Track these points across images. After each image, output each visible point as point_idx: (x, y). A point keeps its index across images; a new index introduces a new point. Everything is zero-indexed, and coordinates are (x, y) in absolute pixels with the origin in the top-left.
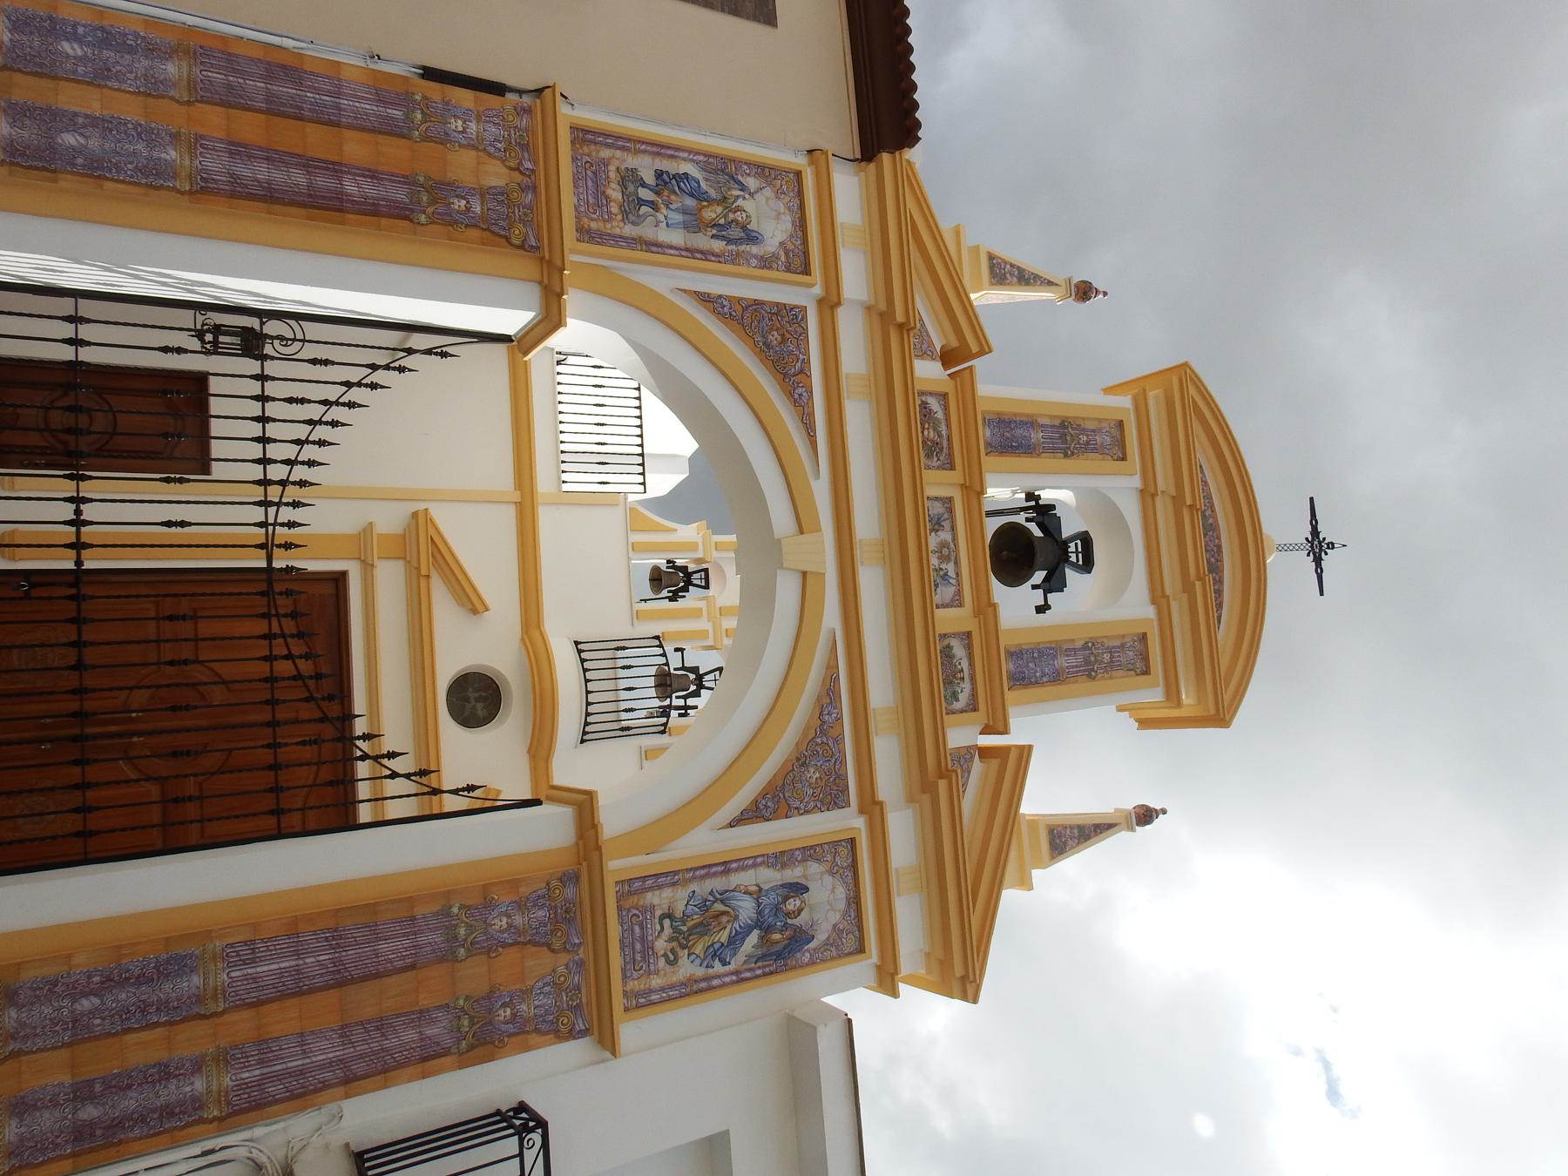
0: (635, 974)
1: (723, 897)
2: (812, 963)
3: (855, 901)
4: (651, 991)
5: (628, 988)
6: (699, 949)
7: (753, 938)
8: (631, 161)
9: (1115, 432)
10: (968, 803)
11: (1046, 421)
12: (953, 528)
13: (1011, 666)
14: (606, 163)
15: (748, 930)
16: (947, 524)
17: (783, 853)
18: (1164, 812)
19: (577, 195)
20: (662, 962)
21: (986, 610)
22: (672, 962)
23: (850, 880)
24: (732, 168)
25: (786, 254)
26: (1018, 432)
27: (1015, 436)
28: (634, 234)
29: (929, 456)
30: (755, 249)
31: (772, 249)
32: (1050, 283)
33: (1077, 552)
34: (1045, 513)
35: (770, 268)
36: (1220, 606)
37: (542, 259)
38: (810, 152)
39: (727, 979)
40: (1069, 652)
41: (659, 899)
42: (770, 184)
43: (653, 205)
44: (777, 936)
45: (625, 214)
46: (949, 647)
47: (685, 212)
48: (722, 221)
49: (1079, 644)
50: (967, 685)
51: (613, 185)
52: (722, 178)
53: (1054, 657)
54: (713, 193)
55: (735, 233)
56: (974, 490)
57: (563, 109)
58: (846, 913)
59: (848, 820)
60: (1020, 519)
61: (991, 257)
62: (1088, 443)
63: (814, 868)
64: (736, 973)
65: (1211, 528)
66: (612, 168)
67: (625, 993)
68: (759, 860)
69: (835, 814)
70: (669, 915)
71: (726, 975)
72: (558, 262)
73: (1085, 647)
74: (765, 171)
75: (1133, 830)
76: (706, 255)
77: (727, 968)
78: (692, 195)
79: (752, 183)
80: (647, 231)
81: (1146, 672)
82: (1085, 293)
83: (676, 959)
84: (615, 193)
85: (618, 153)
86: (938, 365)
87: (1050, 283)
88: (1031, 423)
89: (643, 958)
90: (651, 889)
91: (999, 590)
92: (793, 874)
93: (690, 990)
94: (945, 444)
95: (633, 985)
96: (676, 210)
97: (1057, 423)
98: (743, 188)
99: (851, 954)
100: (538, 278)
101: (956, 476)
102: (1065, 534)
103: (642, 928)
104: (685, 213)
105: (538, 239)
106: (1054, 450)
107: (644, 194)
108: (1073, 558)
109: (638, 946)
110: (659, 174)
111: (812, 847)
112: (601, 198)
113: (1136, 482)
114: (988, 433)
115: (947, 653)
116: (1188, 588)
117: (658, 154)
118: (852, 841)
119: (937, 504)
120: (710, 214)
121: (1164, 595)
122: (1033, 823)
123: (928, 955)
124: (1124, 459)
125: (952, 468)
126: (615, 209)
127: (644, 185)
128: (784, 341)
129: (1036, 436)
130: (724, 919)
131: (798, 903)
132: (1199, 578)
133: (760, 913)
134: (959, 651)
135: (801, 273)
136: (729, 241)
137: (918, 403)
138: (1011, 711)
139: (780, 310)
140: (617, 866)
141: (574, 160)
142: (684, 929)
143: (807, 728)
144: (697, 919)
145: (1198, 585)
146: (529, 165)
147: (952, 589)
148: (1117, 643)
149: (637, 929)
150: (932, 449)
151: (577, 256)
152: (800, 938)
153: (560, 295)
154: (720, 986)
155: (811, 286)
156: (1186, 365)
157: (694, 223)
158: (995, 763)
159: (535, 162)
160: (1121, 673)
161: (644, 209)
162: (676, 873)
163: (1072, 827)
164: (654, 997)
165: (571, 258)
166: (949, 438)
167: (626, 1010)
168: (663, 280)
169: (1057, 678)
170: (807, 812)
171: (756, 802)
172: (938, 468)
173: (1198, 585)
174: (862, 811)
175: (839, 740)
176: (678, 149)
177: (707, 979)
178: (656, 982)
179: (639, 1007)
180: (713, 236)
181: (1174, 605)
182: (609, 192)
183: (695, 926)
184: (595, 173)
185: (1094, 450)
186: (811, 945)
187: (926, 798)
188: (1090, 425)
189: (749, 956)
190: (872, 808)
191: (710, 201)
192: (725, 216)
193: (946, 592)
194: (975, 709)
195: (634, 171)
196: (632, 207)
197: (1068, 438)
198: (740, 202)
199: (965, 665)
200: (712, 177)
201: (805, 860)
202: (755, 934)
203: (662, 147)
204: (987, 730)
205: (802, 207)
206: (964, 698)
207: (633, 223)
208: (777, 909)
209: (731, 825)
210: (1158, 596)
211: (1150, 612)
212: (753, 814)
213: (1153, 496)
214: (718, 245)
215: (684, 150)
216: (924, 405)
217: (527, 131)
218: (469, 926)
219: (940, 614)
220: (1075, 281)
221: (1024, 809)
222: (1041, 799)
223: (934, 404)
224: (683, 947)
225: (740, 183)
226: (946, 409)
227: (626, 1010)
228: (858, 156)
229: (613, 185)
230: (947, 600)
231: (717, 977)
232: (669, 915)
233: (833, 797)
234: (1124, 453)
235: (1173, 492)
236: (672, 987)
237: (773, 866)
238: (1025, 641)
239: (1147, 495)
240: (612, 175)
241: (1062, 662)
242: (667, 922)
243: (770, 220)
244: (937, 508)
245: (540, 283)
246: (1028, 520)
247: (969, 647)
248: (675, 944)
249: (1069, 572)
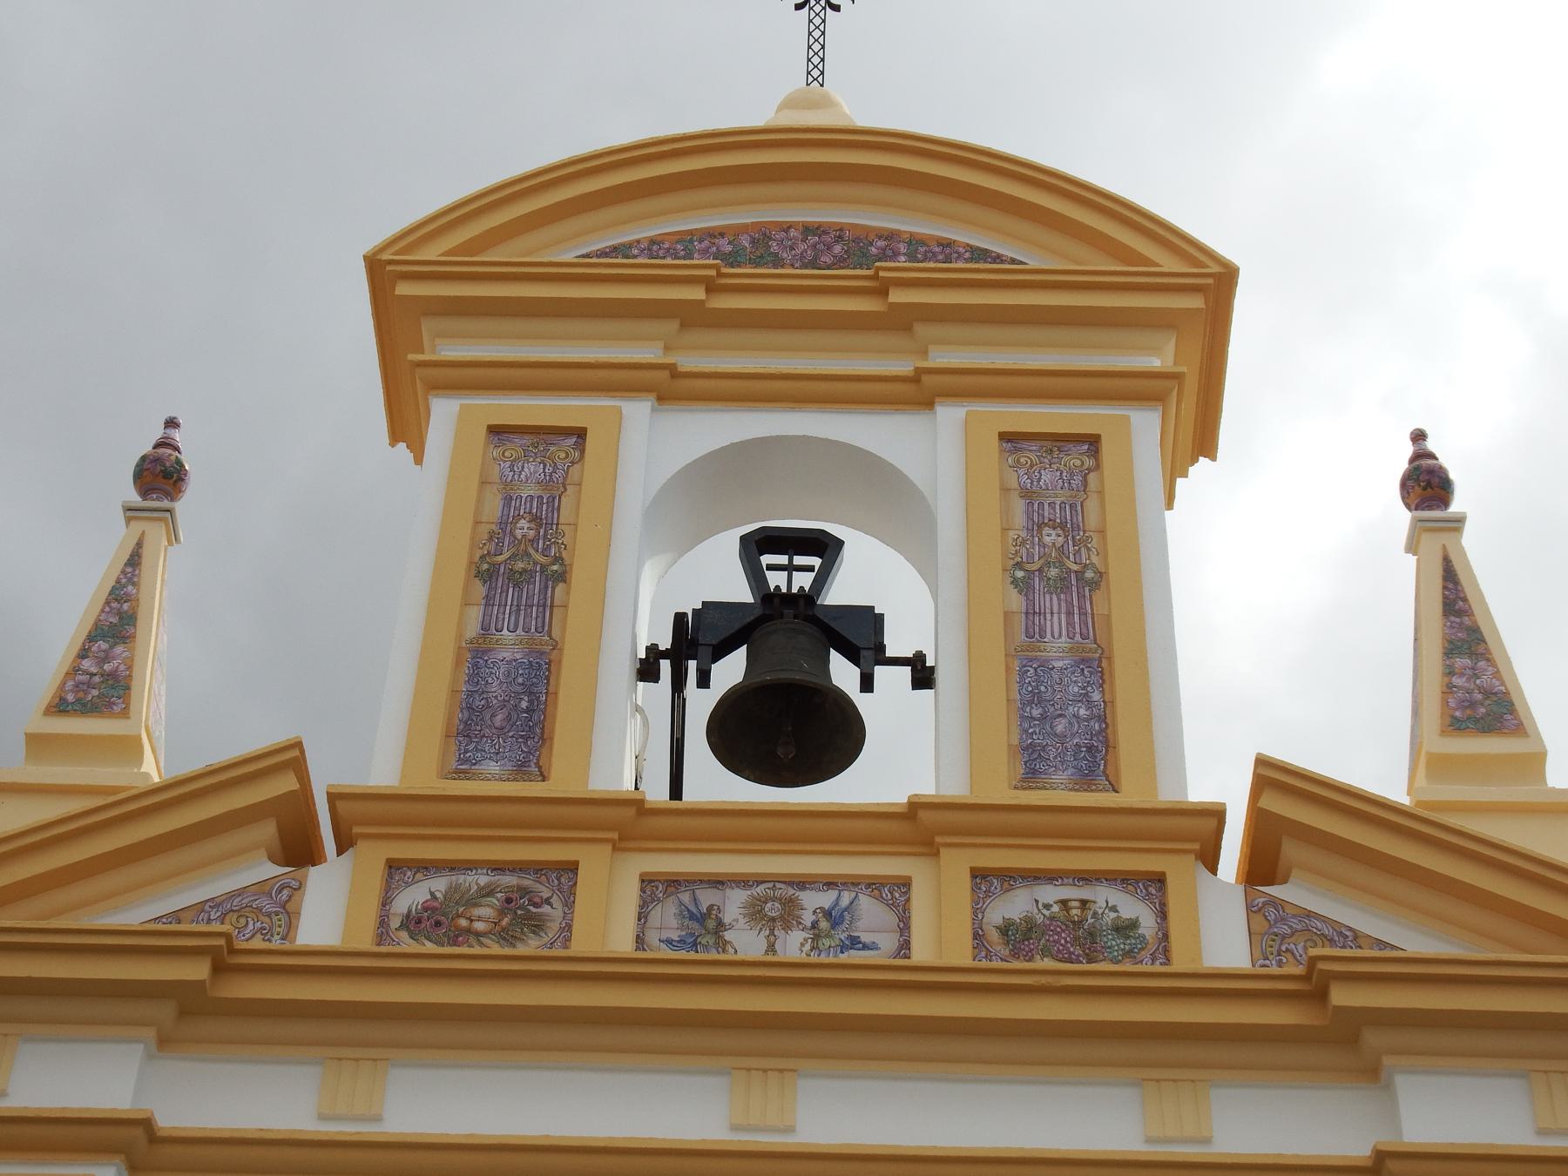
9: (515, 447)
10: (1415, 941)
11: (475, 614)
12: (718, 882)
13: (1061, 777)
16: (707, 898)
18: (1419, 436)
21: (918, 826)
26: (495, 688)
27: (505, 700)
29: (537, 925)
32: (134, 560)
33: (790, 568)
34: (696, 639)
36: (947, 249)
40: (1035, 632)
46: (1006, 929)
49: (1016, 601)
50: (1102, 895)
53: (1044, 665)
56: (626, 822)
60: (701, 704)
61: (59, 707)
62: (536, 519)
65: (762, 245)
73: (1024, 587)
75: (1458, 522)
81: (1092, 443)
82: (167, 475)
86: (314, 872)
87: (134, 560)
88: (477, 655)
91: (872, 781)
94: (510, 880)
97: (480, 590)
101: (593, 861)
102: (741, 593)
106: (546, 605)
108: (803, 581)
113: (637, 412)
114: (492, 767)
115: (1020, 936)
116: (902, 322)
119: (656, 915)
121: (916, 377)
122: (1427, 763)
124: (580, 434)
125: (572, 868)
129: (509, 645)
132: (882, 291)
134: (1015, 905)
137: (407, 944)
138: (1166, 795)
145: (897, 296)
147: (866, 903)
148: (1019, 506)
150: (521, 915)
156: (382, 272)
158: (1291, 850)
160: (1092, 506)
163: (1450, 672)
166: (498, 867)
169: (1094, 664)
172: (569, 904)
173: (897, 296)
181: (942, 358)
185: (554, 503)
187: (1373, 1039)
188: (493, 507)
193: (872, 917)
194: (1159, 880)
197: (520, 568)
199: (1050, 894)
204: (1210, 860)
206: (1130, 907)
210: (917, 394)
211: (950, 416)
213: (674, 372)
216: (413, 923)
219: (921, 953)
220: (134, 498)
221: (1398, 794)
222: (1371, 747)
223: (412, 897)
226: (426, 867)
230: (891, 919)
234: (565, 432)
235: (672, 326)
238: (1003, 734)
239: (672, 389)
241: (1057, 646)
244: (667, 919)
246: (704, 681)
247: (1011, 878)
249: (835, 595)
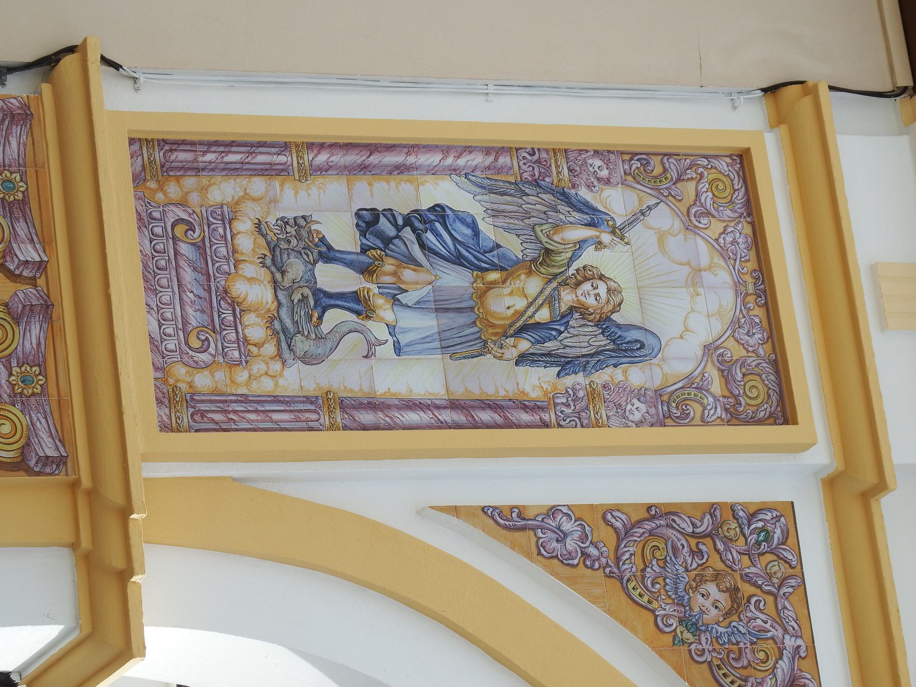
8: (293, 200)
14: (227, 216)
19: (157, 310)
24: (561, 174)
25: (726, 376)
28: (311, 388)
30: (636, 376)
31: (685, 368)
35: (683, 419)
37: (74, 485)
38: (771, 90)
42: (665, 196)
43: (357, 303)
45: (284, 338)
47: (441, 306)
48: (543, 315)
51: (250, 270)
52: (535, 202)
54: (513, 246)
55: (582, 339)
57: (114, 99)
66: (244, 226)
72: (113, 493)
74: (650, 166)
76: (504, 413)
78: (458, 260)
79: (616, 201)
80: (344, 373)
84: (254, 289)
85: (258, 185)
96: (419, 306)
98: (594, 217)
100: (69, 537)
104: (441, 309)
105: (62, 437)
107: (333, 278)
110: (368, 221)
112: (222, 306)
117: (364, 168)
120: (507, 302)
126: (255, 329)
127: (328, 255)
128: (737, 604)
135: (773, 419)
136: (566, 364)
139: (719, 523)
141: (144, 221)
146: (29, 253)
151: (162, 464)
153: (124, 575)
155: (806, 447)
157: (470, 333)
159: (45, 241)
161: (334, 317)
165: (145, 471)
168: (395, 489)
176: (412, 148)
178: (242, 381)
180: (523, 359)
182: (239, 288)
184: (200, 247)
191: (508, 268)
192: (551, 301)
195: (301, 223)
196: (303, 315)
198: (589, 257)
200: (507, 203)
203: (373, 148)
205: (758, 241)
207: (307, 359)
214: (536, 381)
215: (429, 148)
217: (21, 166)
218: (745, 644)
225: (585, 208)
228: (904, 79)
229: (250, 270)
240: (246, 242)
243: (672, 290)
245: (74, 546)
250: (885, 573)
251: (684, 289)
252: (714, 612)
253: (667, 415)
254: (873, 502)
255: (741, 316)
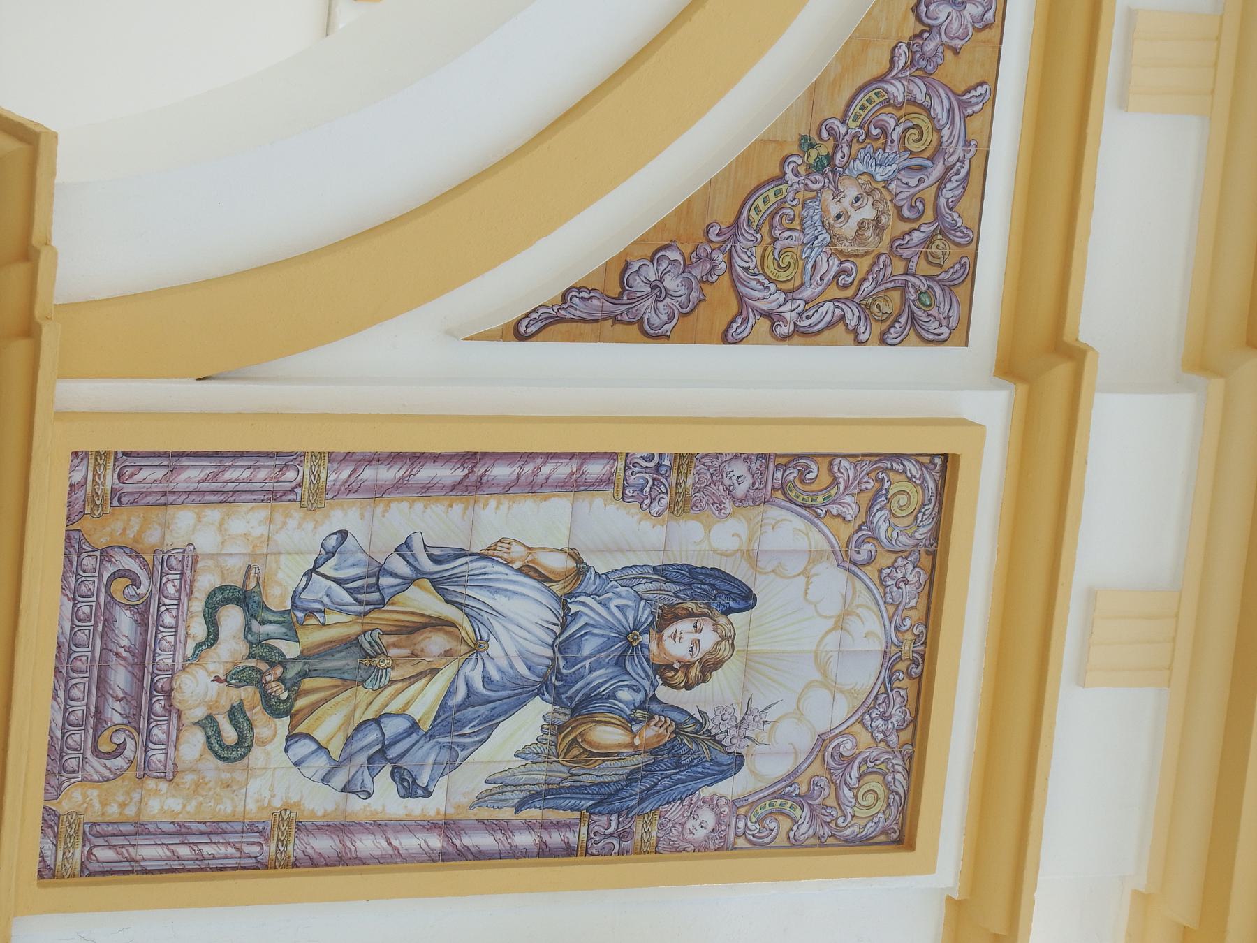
0: (96, 766)
1: (445, 570)
2: (718, 845)
3: (912, 672)
4: (141, 830)
5: (64, 806)
6: (329, 725)
7: (528, 723)
15: (519, 694)
17: (684, 460)
20: (193, 744)
22: (233, 749)
23: (910, 594)
39: (409, 843)
41: (221, 539)
44: (608, 735)
58: (870, 708)
59: (943, 390)
63: (787, 531)
64: (446, 827)
67: (51, 821)
68: (595, 469)
69: (910, 359)
70: (244, 597)
71: (408, 826)
77: (417, 807)
83: (244, 744)
89: (133, 719)
90: (195, 497)
92: (707, 540)
93: (273, 853)
95: (79, 799)
99: (861, 842)
103: (142, 623)
109: (120, 678)
111: (796, 458)
118: (946, 465)
123: (1142, 900)
130: (435, 643)
131: (708, 639)
133: (563, 647)
140: (89, 401)
142: (290, 650)
143: (861, 40)
144: (339, 626)
149: (125, 623)
152: (691, 754)
154: (380, 861)
162: (290, 460)
164: (149, 852)
167: (46, 873)
170: (802, 334)
171: (623, 267)
174: (1009, 367)
175: (974, 100)
177: (340, 827)
178: (163, 804)
179: (91, 871)
183: (330, 649)
186: (728, 788)
189: (500, 784)
190: (1046, 358)
201: (758, 499)
202: (537, 712)
208: (627, 646)
209: (517, 332)
212: (610, 305)
224: (274, 708)
227: (46, 873)
231: (376, 826)
232: (244, 597)
233: (911, 297)
236: (215, 830)
237: (641, 498)
242: (232, 618)
248: (248, 694)
250: (1090, 130)
251: (814, 648)
252: (834, 209)
253: (740, 833)
254: (1068, 338)
255: (882, 690)
